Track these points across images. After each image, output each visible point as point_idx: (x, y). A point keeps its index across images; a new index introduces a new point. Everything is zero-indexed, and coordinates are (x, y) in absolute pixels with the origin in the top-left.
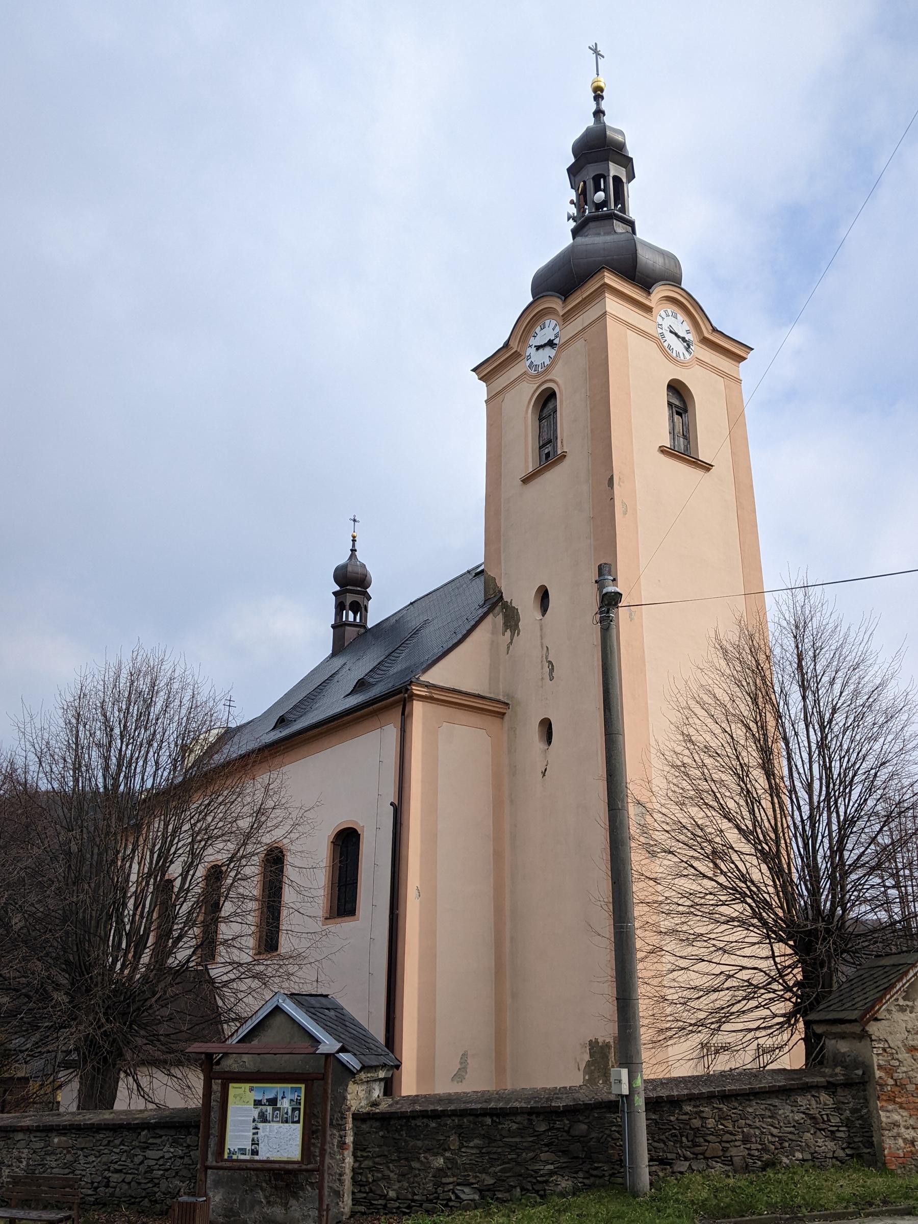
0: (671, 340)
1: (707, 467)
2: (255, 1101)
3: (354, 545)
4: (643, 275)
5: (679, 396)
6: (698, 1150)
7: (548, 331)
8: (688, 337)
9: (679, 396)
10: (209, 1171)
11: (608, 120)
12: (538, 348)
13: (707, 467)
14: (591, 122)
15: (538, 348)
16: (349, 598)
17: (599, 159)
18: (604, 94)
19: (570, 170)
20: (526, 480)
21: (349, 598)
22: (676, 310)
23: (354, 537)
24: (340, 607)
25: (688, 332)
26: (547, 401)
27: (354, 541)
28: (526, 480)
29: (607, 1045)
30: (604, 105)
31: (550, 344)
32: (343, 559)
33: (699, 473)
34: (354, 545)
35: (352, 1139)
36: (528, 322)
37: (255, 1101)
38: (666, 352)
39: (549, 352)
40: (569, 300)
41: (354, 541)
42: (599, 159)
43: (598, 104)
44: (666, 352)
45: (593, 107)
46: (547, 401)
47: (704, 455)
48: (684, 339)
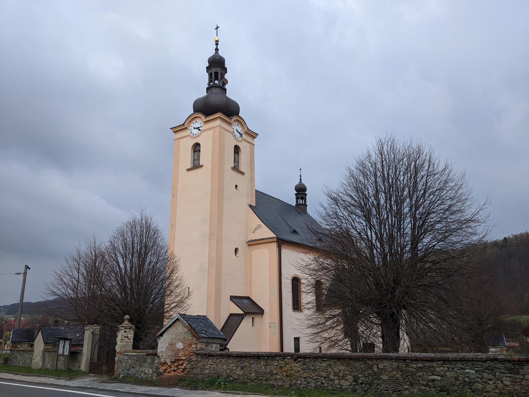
0: (236, 133)
1: (243, 173)
2: (299, 338)
4: (230, 111)
5: (237, 149)
7: (198, 123)
8: (241, 132)
9: (237, 149)
10: (70, 368)
12: (195, 128)
13: (243, 173)
14: (213, 52)
15: (195, 128)
16: (300, 196)
17: (217, 67)
19: (207, 67)
20: (188, 170)
21: (300, 196)
24: (297, 199)
26: (196, 148)
27: (217, 44)
28: (188, 170)
31: (198, 128)
32: (297, 182)
36: (191, 119)
37: (299, 338)
39: (197, 130)
41: (217, 44)
42: (217, 67)
43: (217, 46)
44: (235, 136)
46: (196, 148)
47: (241, 169)
48: (240, 133)
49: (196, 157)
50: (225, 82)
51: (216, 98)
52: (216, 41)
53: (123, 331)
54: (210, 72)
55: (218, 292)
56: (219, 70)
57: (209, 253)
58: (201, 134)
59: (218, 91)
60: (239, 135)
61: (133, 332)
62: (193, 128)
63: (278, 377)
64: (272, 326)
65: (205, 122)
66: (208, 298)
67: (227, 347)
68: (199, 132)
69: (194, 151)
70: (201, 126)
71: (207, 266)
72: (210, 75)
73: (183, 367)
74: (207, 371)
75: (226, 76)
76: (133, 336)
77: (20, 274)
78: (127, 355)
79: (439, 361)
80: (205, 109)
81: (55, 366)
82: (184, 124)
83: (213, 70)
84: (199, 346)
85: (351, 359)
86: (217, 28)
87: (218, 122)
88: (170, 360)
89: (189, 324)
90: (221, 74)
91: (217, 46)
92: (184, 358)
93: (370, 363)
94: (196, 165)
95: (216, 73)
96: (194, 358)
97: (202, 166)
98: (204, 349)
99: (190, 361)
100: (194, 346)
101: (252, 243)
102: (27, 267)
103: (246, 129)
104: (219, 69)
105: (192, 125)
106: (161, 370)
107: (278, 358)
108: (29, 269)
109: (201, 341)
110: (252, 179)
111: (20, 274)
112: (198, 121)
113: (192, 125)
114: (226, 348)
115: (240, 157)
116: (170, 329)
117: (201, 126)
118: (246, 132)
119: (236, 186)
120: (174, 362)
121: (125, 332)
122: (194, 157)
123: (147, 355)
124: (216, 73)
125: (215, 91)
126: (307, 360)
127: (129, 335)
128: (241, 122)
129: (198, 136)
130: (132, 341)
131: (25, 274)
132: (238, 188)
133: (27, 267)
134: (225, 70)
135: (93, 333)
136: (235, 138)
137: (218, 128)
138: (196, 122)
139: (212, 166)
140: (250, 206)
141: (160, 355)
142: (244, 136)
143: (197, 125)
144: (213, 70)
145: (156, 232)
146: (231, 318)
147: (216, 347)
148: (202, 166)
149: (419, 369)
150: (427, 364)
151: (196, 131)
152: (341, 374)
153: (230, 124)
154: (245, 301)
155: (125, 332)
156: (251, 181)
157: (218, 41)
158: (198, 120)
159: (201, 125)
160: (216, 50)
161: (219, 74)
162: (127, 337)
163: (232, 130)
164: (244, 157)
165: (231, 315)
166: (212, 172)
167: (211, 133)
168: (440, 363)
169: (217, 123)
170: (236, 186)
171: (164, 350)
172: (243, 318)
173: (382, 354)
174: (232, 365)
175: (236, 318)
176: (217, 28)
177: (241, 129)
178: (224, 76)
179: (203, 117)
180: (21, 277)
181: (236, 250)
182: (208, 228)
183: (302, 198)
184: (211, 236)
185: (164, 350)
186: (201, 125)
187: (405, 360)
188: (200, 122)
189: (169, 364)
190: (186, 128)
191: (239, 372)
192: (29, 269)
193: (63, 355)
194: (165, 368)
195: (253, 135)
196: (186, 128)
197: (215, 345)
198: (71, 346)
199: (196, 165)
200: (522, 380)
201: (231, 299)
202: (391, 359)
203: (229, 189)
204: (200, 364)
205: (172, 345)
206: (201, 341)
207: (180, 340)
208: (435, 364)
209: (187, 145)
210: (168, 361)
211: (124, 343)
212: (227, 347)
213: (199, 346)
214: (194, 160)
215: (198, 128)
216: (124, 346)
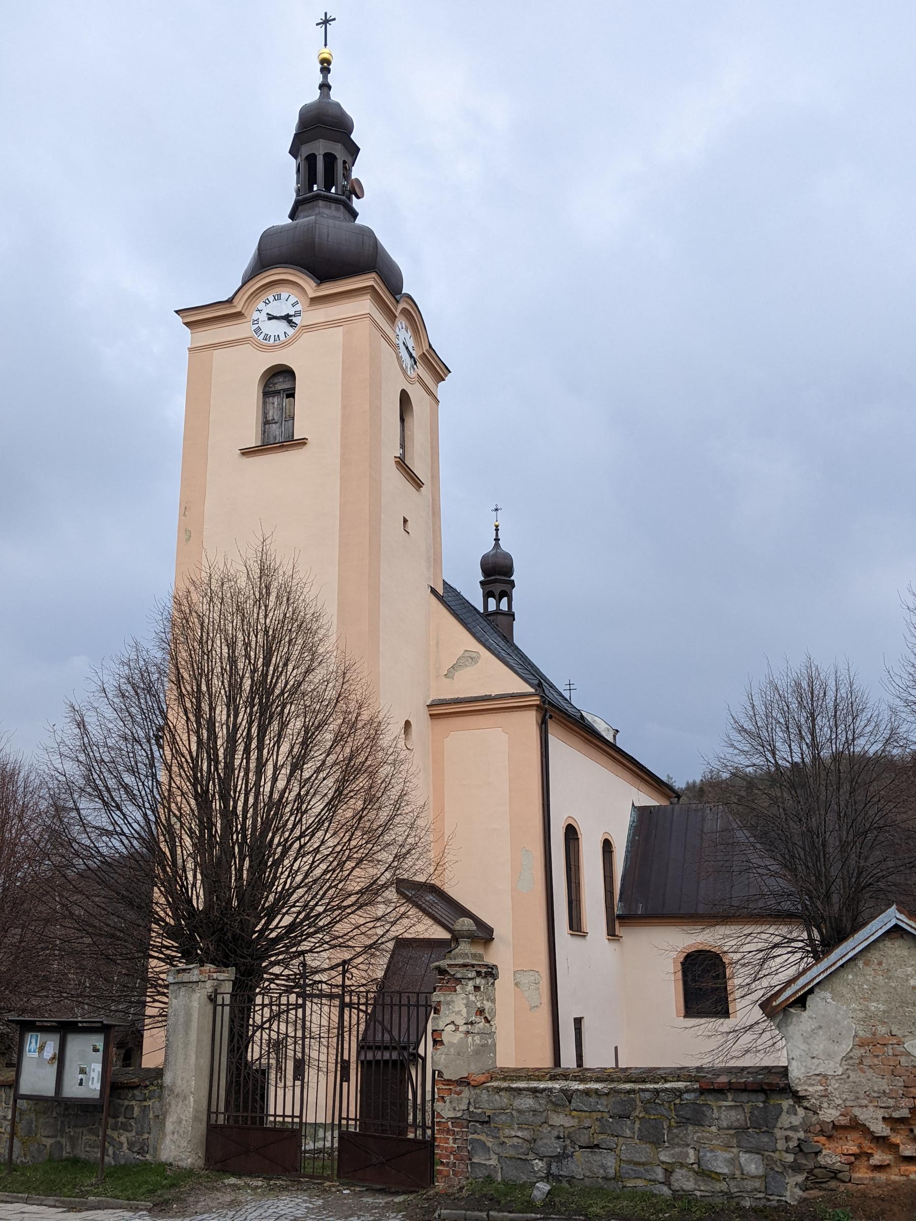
3: (497, 535)
5: (405, 399)
6: (595, 1115)
11: (335, 96)
12: (271, 317)
15: (271, 317)
17: (324, 143)
18: (319, 66)
20: (247, 452)
23: (497, 526)
26: (279, 383)
27: (497, 530)
28: (247, 452)
30: (331, 79)
31: (287, 318)
33: (410, 488)
34: (497, 535)
35: (255, 764)
39: (283, 326)
40: (324, 286)
41: (497, 530)
42: (324, 143)
43: (325, 77)
45: (319, 78)
46: (279, 383)
50: (356, 190)
53: (470, 987)
54: (306, 150)
58: (295, 338)
59: (334, 213)
62: (263, 317)
64: (524, 980)
65: (315, 301)
68: (291, 331)
69: (268, 393)
70: (298, 314)
75: (356, 173)
78: (535, 1091)
82: (230, 301)
86: (326, 22)
88: (880, 1114)
91: (325, 77)
94: (277, 438)
97: (302, 442)
101: (444, 710)
105: (261, 305)
112: (284, 295)
113: (261, 305)
117: (298, 314)
121: (477, 988)
122: (265, 414)
123: (702, 1091)
124: (330, 159)
125: (326, 211)
129: (284, 345)
132: (499, 507)
134: (354, 150)
138: (278, 298)
148: (302, 442)
151: (279, 328)
156: (434, 514)
157: (329, 62)
160: (321, 87)
166: (345, 462)
167: (325, 338)
176: (326, 22)
178: (347, 171)
185: (833, 1067)
186: (298, 307)
188: (293, 299)
190: (239, 315)
196: (239, 315)
199: (277, 438)
209: (246, 369)
214: (266, 422)
215: (287, 318)
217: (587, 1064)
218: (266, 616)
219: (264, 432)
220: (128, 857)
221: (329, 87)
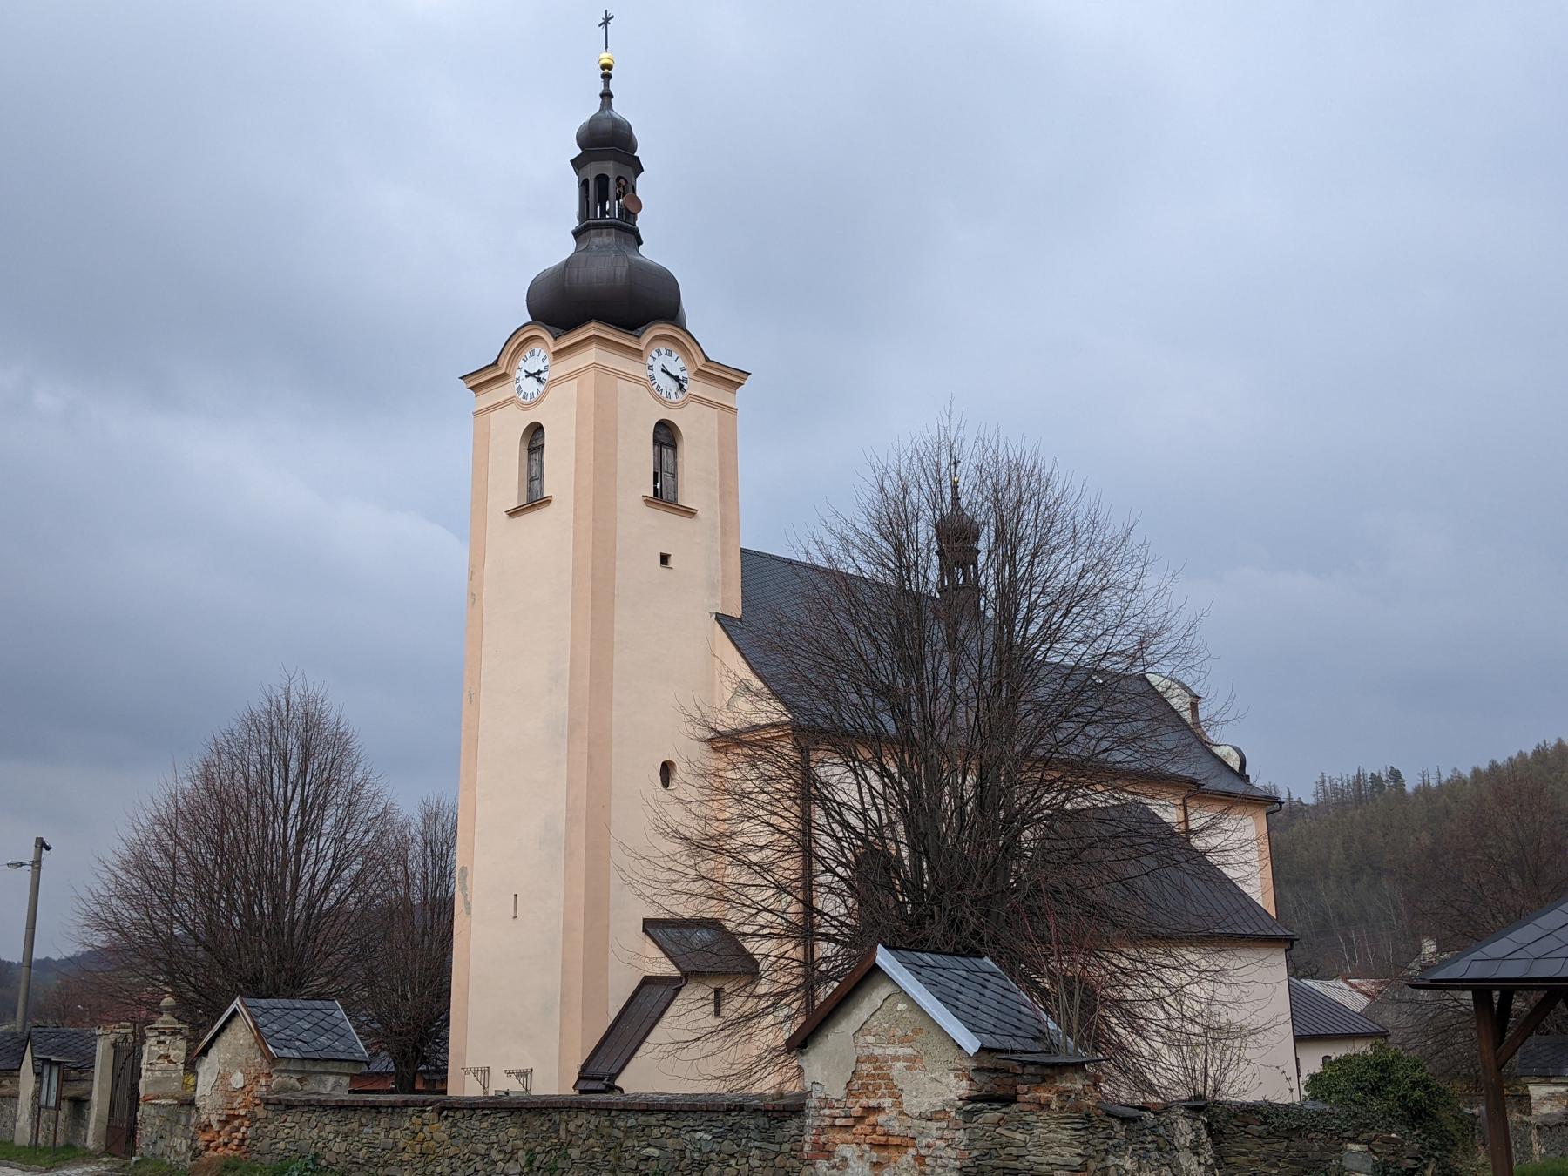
1: (690, 513)
5: (666, 436)
7: (537, 358)
9: (666, 436)
12: (529, 375)
13: (690, 513)
14: (595, 106)
15: (529, 375)
17: (607, 155)
20: (513, 513)
22: (670, 347)
25: (683, 369)
26: (535, 434)
27: (607, 77)
28: (513, 513)
29: (444, 1092)
30: (614, 86)
31: (536, 375)
36: (518, 343)
38: (656, 393)
41: (607, 77)
42: (607, 155)
43: (607, 85)
44: (656, 393)
45: (600, 88)
46: (535, 434)
47: (685, 500)
48: (676, 378)
49: (535, 470)
51: (606, 266)
52: (604, 67)
55: (596, 907)
56: (610, 169)
57: (570, 783)
60: (673, 385)
61: (183, 1044)
62: (521, 374)
63: (406, 1157)
65: (555, 353)
66: (567, 928)
67: (617, 1083)
68: (542, 388)
70: (546, 369)
71: (562, 827)
72: (584, 184)
73: (239, 1135)
74: (282, 1145)
76: (183, 1054)
77: (22, 864)
79: (661, 1111)
80: (561, 308)
81: (51, 1137)
83: (593, 170)
84: (276, 1080)
85: (529, 1110)
86: (606, 22)
87: (591, 354)
89: (255, 1024)
90: (619, 178)
91: (607, 85)
92: (242, 1112)
93: (556, 1117)
95: (602, 180)
96: (260, 1112)
97: (548, 501)
98: (294, 1089)
99: (253, 1119)
100: (263, 1081)
102: (42, 845)
103: (700, 362)
104: (611, 164)
106: (200, 1144)
107: (410, 1111)
108: (48, 848)
109: (280, 1067)
110: (728, 525)
111: (22, 864)
112: (537, 351)
114: (611, 1088)
115: (679, 459)
116: (223, 1037)
118: (700, 373)
119: (664, 559)
120: (226, 1122)
122: (530, 471)
125: (597, 240)
126: (459, 1115)
127: (172, 1053)
128: (685, 343)
130: (181, 1067)
131: (37, 864)
132: (672, 562)
133: (42, 845)
135: (114, 1045)
136: (658, 398)
137: (592, 372)
139: (576, 501)
140: (721, 619)
141: (200, 1103)
142: (695, 387)
143: (534, 364)
144: (593, 170)
145: (340, 740)
146: (646, 989)
147: (337, 1085)
148: (548, 501)
149: (628, 1131)
150: (642, 1119)
151: (531, 386)
152: (508, 1149)
153: (638, 354)
154: (705, 935)
155: (159, 1042)
157: (610, 67)
158: (537, 348)
159: (547, 362)
160: (602, 96)
161: (612, 183)
162: (167, 1057)
163: (643, 373)
164: (693, 459)
165: (647, 981)
168: (662, 1116)
169: (593, 357)
170: (664, 559)
171: (208, 1092)
172: (679, 990)
173: (1309, 1106)
174: (328, 1128)
175: (659, 992)
176: (606, 22)
177: (681, 363)
179: (548, 338)
180: (26, 874)
181: (667, 769)
182: (566, 704)
183: (964, 565)
184: (573, 725)
185: (208, 1092)
186: (547, 362)
187: (610, 1110)
188: (543, 354)
189: (216, 1126)
190: (504, 376)
191: (339, 1146)
192: (48, 848)
193: (46, 1107)
194: (207, 1138)
195: (732, 379)
197: (331, 1080)
198: (64, 1080)
200: (778, 1154)
201: (644, 930)
202: (597, 1109)
203: (635, 567)
204: (271, 1127)
205: (223, 1078)
206: (280, 1067)
207: (239, 1065)
208: (653, 1120)
209: (511, 427)
210: (214, 1118)
211: (158, 1074)
212: (617, 1083)
213: (276, 1080)
214: (531, 480)
215: (536, 375)
216: (156, 1082)
217: (38, 955)
218: (1065, 616)
219: (529, 489)
220: (1425, 935)
221: (611, 96)
